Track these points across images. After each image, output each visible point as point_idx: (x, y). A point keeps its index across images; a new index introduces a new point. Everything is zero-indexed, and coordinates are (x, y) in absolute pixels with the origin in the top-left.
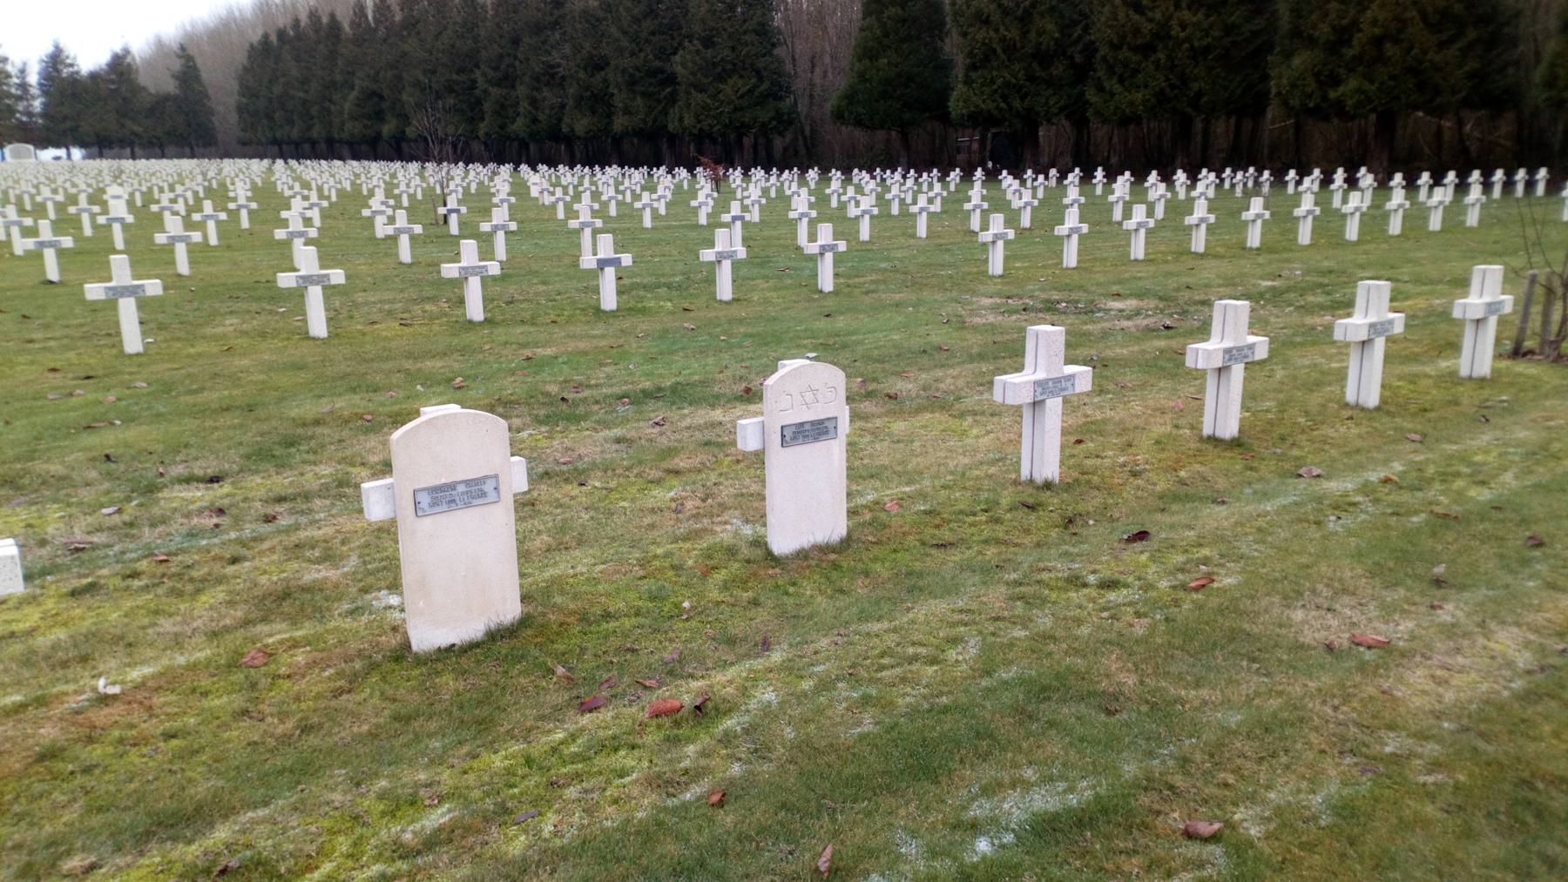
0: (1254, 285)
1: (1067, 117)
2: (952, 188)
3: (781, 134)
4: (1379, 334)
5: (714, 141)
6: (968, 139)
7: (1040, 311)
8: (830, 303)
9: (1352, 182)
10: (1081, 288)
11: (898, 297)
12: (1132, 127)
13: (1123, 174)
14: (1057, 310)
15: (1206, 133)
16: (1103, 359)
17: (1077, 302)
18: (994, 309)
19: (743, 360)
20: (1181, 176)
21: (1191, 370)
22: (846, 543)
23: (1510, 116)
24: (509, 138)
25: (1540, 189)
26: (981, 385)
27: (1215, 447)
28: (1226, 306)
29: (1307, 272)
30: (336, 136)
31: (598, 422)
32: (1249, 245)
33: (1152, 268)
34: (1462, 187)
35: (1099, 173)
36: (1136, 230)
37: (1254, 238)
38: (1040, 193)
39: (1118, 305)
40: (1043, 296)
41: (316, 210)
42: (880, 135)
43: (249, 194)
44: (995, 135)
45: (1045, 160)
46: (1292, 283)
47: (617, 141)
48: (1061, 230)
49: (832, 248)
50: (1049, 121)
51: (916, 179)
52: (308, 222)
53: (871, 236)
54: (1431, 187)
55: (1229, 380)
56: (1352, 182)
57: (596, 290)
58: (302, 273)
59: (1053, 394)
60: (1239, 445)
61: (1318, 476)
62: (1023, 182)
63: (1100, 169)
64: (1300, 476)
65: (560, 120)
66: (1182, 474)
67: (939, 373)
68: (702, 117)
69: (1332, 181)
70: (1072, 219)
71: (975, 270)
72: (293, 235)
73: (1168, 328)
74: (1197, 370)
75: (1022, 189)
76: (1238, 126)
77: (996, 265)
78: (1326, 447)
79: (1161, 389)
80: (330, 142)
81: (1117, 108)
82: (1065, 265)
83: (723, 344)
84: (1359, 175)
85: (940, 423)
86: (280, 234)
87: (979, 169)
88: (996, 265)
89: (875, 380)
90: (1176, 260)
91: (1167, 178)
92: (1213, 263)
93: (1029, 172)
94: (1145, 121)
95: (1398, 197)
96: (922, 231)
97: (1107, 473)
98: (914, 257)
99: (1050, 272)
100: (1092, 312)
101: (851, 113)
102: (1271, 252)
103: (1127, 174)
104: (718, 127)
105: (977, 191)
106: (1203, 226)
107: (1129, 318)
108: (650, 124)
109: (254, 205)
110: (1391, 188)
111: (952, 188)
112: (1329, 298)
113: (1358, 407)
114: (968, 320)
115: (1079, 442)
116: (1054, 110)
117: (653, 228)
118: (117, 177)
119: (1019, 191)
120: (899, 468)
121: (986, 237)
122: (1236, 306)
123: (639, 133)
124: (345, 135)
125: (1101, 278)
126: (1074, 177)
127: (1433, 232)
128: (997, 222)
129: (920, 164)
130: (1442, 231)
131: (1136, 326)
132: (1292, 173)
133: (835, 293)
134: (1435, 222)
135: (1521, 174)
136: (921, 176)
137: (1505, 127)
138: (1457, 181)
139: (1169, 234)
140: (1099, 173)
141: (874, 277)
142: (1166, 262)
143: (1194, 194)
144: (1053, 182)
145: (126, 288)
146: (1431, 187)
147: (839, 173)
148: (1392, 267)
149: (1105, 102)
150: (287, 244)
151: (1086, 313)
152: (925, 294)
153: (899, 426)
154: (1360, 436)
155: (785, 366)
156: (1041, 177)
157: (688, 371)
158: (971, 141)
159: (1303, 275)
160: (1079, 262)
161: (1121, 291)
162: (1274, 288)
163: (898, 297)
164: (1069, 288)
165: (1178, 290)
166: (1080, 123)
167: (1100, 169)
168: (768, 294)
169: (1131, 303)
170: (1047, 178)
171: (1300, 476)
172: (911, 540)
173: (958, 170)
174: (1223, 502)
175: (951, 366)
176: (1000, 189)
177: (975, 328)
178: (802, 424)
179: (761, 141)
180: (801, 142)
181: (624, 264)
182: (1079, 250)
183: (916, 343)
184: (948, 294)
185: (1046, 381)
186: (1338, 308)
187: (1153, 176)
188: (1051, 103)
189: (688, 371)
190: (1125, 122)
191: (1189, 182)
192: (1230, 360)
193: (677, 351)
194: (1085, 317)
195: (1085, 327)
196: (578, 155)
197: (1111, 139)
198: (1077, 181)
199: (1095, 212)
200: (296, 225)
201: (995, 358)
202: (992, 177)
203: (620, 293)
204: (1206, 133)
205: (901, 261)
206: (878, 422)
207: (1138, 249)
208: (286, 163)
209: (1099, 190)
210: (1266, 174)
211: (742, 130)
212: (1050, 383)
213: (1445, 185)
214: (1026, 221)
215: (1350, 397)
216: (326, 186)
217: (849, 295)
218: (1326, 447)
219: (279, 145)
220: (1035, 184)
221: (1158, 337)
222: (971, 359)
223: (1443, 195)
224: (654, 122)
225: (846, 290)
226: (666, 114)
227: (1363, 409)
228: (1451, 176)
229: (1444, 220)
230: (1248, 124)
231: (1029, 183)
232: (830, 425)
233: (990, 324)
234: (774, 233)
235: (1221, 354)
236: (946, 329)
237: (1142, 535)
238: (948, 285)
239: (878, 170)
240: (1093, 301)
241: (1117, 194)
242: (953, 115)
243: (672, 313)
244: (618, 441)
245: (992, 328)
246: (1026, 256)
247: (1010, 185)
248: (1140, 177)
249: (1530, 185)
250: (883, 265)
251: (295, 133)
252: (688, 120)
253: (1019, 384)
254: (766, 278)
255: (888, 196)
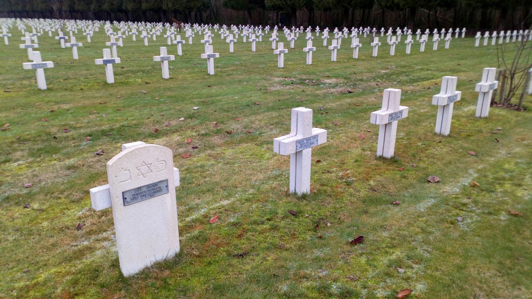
0: (379, 72)
1: (306, 8)
2: (266, 32)
3: (205, 11)
4: (451, 101)
5: (180, 13)
6: (272, 15)
7: (298, 84)
8: (212, 80)
9: (394, 33)
10: (314, 73)
11: (241, 77)
12: (328, 12)
13: (326, 28)
14: (305, 83)
15: (353, 14)
16: (326, 109)
17: (313, 80)
18: (280, 83)
19: (162, 111)
20: (346, 30)
21: (373, 125)
22: (179, 256)
23: (452, 9)
24: (102, 11)
25: (463, 35)
26: (272, 125)
27: (384, 163)
28: (390, 92)
29: (397, 67)
30: (36, 9)
31: (65, 154)
32: (373, 55)
33: (340, 65)
34: (431, 34)
35: (318, 28)
36: (375, 46)
37: (375, 53)
38: (297, 35)
39: (328, 81)
40: (299, 77)
41: (36, 37)
42: (241, 12)
43: (8, 30)
44: (282, 14)
45: (299, 23)
46: (392, 71)
47: (144, 12)
48: (306, 49)
49: (213, 56)
50: (300, 9)
51: (254, 29)
52: (33, 42)
53: (234, 51)
54: (421, 35)
55: (391, 129)
56: (394, 33)
57: (104, 74)
58: (34, 63)
59: (306, 147)
60: (396, 162)
61: (438, 182)
62: (291, 31)
63: (318, 27)
64: (429, 182)
65: (122, 4)
66: (372, 182)
67: (253, 118)
68: (175, 4)
69: (387, 32)
70: (310, 45)
71: (273, 65)
72: (27, 47)
73: (350, 92)
74: (376, 125)
75: (291, 33)
76: (364, 13)
77: (281, 63)
78: (435, 160)
79: (353, 126)
80: (34, 11)
81: (323, 5)
82: (307, 63)
83: (157, 101)
84: (397, 30)
85: (250, 149)
86: (22, 46)
87: (276, 26)
88: (281, 63)
89: (222, 122)
90: (348, 61)
91: (340, 30)
92: (362, 63)
93: (294, 27)
94: (332, 10)
95: (436, 37)
96: (254, 49)
97: (334, 184)
98: (250, 59)
99: (302, 66)
100: (318, 84)
101: (230, 4)
102: (381, 58)
103: (327, 28)
104: (181, 8)
105: (275, 33)
106: (358, 48)
107: (333, 87)
108: (156, 6)
109: (10, 35)
110: (417, 35)
111: (266, 32)
112: (408, 78)
113: (440, 135)
114: (268, 88)
115: (319, 161)
116: (302, 5)
117: (149, 46)
118: (29, 29)
119: (290, 34)
120: (224, 184)
121: (277, 52)
122: (395, 92)
123: (151, 10)
124: (39, 9)
125: (321, 69)
126: (309, 29)
127: (435, 50)
128: (281, 45)
129: (255, 23)
130: (437, 50)
131: (337, 91)
132: (383, 29)
133: (215, 75)
134: (422, 48)
135: (458, 30)
136: (255, 28)
137: (450, 14)
138: (429, 32)
139: (344, 51)
140: (318, 28)
141: (233, 68)
142: (344, 62)
143: (351, 36)
144: (302, 31)
145: (39, 64)
146: (421, 35)
147: (225, 26)
148: (427, 65)
149: (319, 2)
150: (25, 50)
151: (316, 85)
152: (253, 76)
153: (229, 152)
154: (447, 153)
155: (125, 148)
156: (298, 29)
157: (132, 118)
158: (273, 16)
159: (396, 67)
160: (312, 62)
161: (329, 75)
162: (386, 74)
163: (241, 77)
164: (309, 73)
165: (351, 74)
166: (311, 10)
167: (318, 27)
168: (186, 76)
169: (333, 81)
170: (299, 30)
171: (429, 182)
172: (222, 252)
173: (268, 26)
174: (397, 204)
175: (259, 114)
176: (283, 33)
177: (272, 93)
178: (139, 188)
179: (198, 14)
180: (213, 14)
181: (116, 62)
182: (313, 57)
183: (246, 100)
184: (262, 76)
185: (303, 140)
186: (413, 82)
187: (336, 30)
188: (301, 2)
189: (132, 118)
190: (326, 10)
191: (348, 32)
192: (392, 119)
193: (132, 105)
194: (316, 87)
195: (317, 92)
196: (130, 17)
197: (321, 16)
198: (310, 30)
199: (317, 42)
200: (28, 43)
201: (279, 109)
202: (280, 29)
203: (115, 74)
204: (353, 14)
205: (244, 61)
206: (219, 150)
207: (334, 57)
208: (21, 20)
209: (318, 34)
210: (374, 29)
211: (190, 9)
212: (305, 141)
213: (425, 34)
214: (292, 45)
215: (437, 130)
216: (38, 28)
217: (221, 76)
218: (435, 160)
219: (14, 13)
220: (296, 31)
221: (346, 97)
222: (269, 109)
223: (425, 37)
224: (157, 6)
225: (220, 74)
226: (162, 3)
227: (443, 136)
228: (427, 31)
229: (438, 46)
230: (367, 11)
231: (293, 31)
232: (163, 185)
233: (278, 91)
234: (197, 49)
235: (388, 116)
236: (259, 93)
237: (359, 240)
238: (262, 72)
239: (240, 25)
240: (319, 80)
241: (325, 36)
242: (267, 5)
243: (140, 85)
244: (69, 168)
245: (278, 93)
246: (293, 59)
247: (287, 32)
248: (332, 30)
249: (460, 34)
250: (237, 63)
251: (20, 8)
252: (170, 5)
253: (288, 143)
254: (187, 68)
255: (242, 35)
